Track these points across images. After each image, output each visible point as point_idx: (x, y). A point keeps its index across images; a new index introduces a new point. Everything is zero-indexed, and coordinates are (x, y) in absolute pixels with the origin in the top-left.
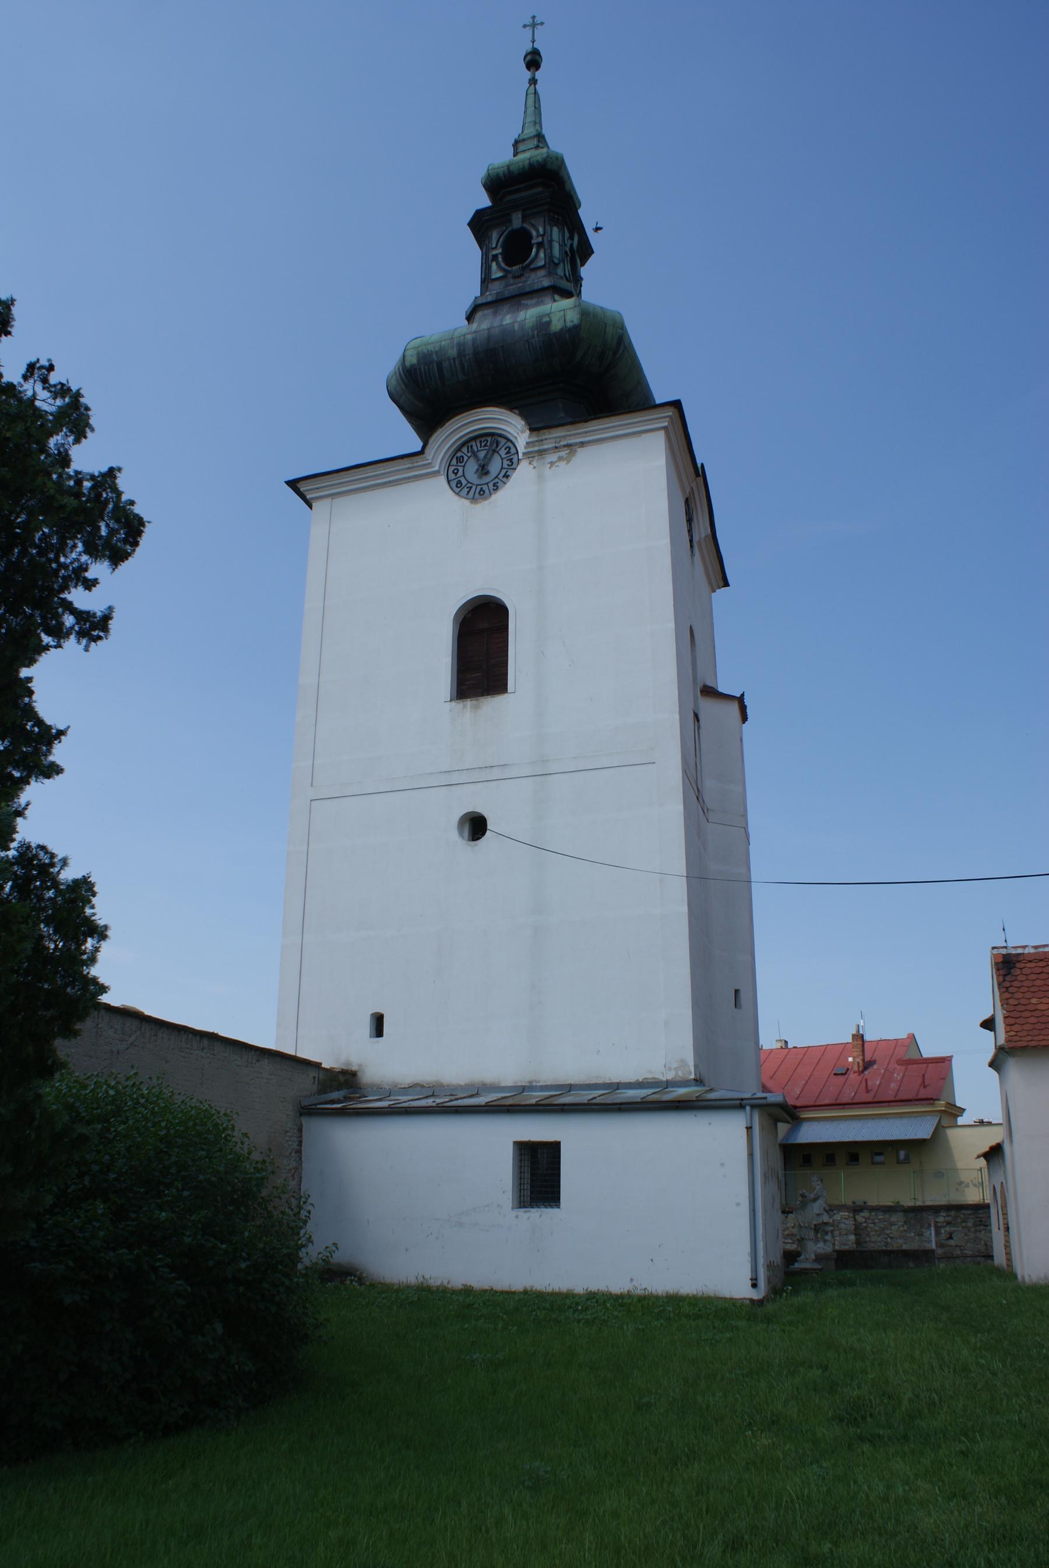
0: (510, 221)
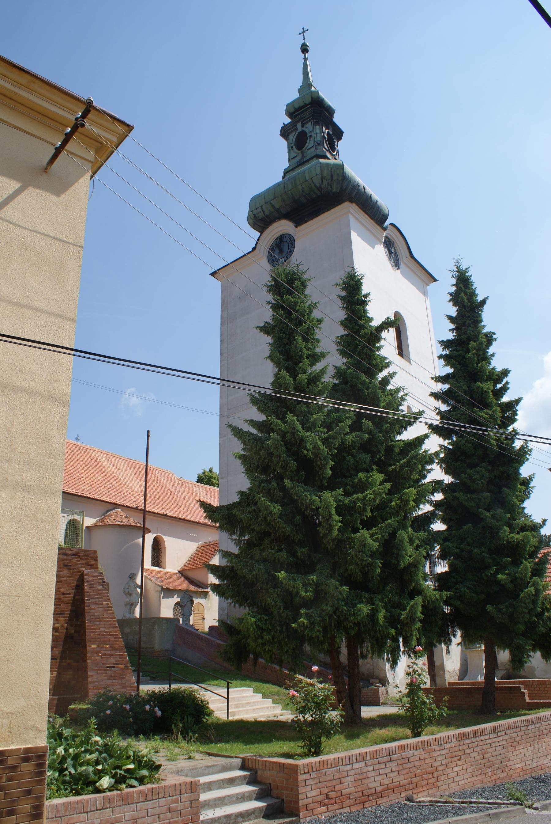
0: (297, 128)
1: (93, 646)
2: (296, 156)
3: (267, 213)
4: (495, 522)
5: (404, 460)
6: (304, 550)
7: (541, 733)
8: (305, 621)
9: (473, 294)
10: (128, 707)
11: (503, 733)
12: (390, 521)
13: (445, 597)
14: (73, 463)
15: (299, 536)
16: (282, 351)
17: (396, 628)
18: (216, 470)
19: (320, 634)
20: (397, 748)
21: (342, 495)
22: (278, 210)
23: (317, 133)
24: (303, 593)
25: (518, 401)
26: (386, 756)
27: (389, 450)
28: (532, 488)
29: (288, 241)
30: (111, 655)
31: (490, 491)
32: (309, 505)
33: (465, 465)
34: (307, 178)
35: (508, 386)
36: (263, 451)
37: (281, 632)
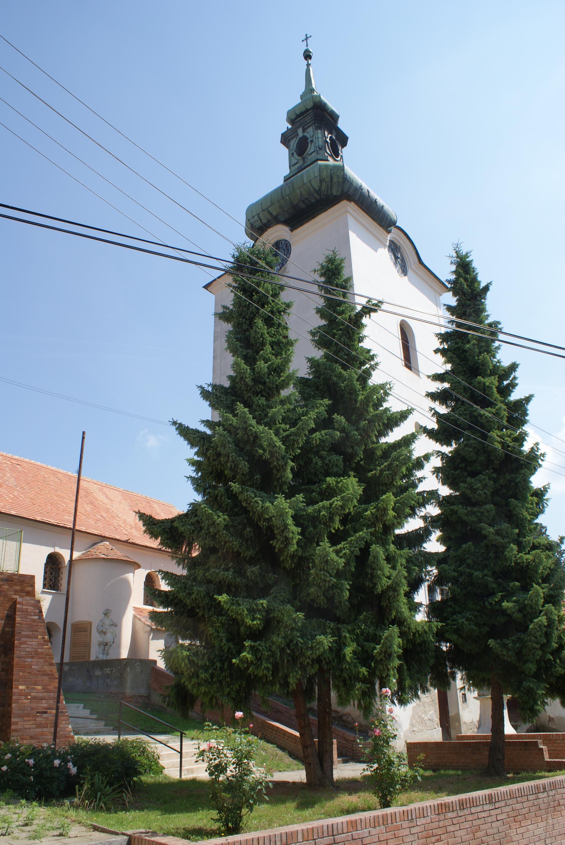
0: (298, 134)
1: (21, 687)
4: (499, 539)
5: (386, 464)
6: (254, 569)
7: (556, 803)
8: (248, 656)
9: (474, 280)
10: (31, 762)
11: (503, 804)
12: (361, 533)
13: (435, 630)
14: (59, 493)
15: (249, 553)
16: (241, 338)
17: (369, 667)
19: (268, 672)
20: (345, 825)
21: (303, 502)
23: (318, 138)
24: (249, 621)
25: (528, 399)
26: (329, 836)
27: (370, 454)
28: (547, 500)
29: (284, 247)
30: (42, 699)
31: (495, 504)
32: (262, 513)
33: (466, 474)
34: (305, 181)
35: (516, 382)
36: (211, 451)
37: (222, 669)
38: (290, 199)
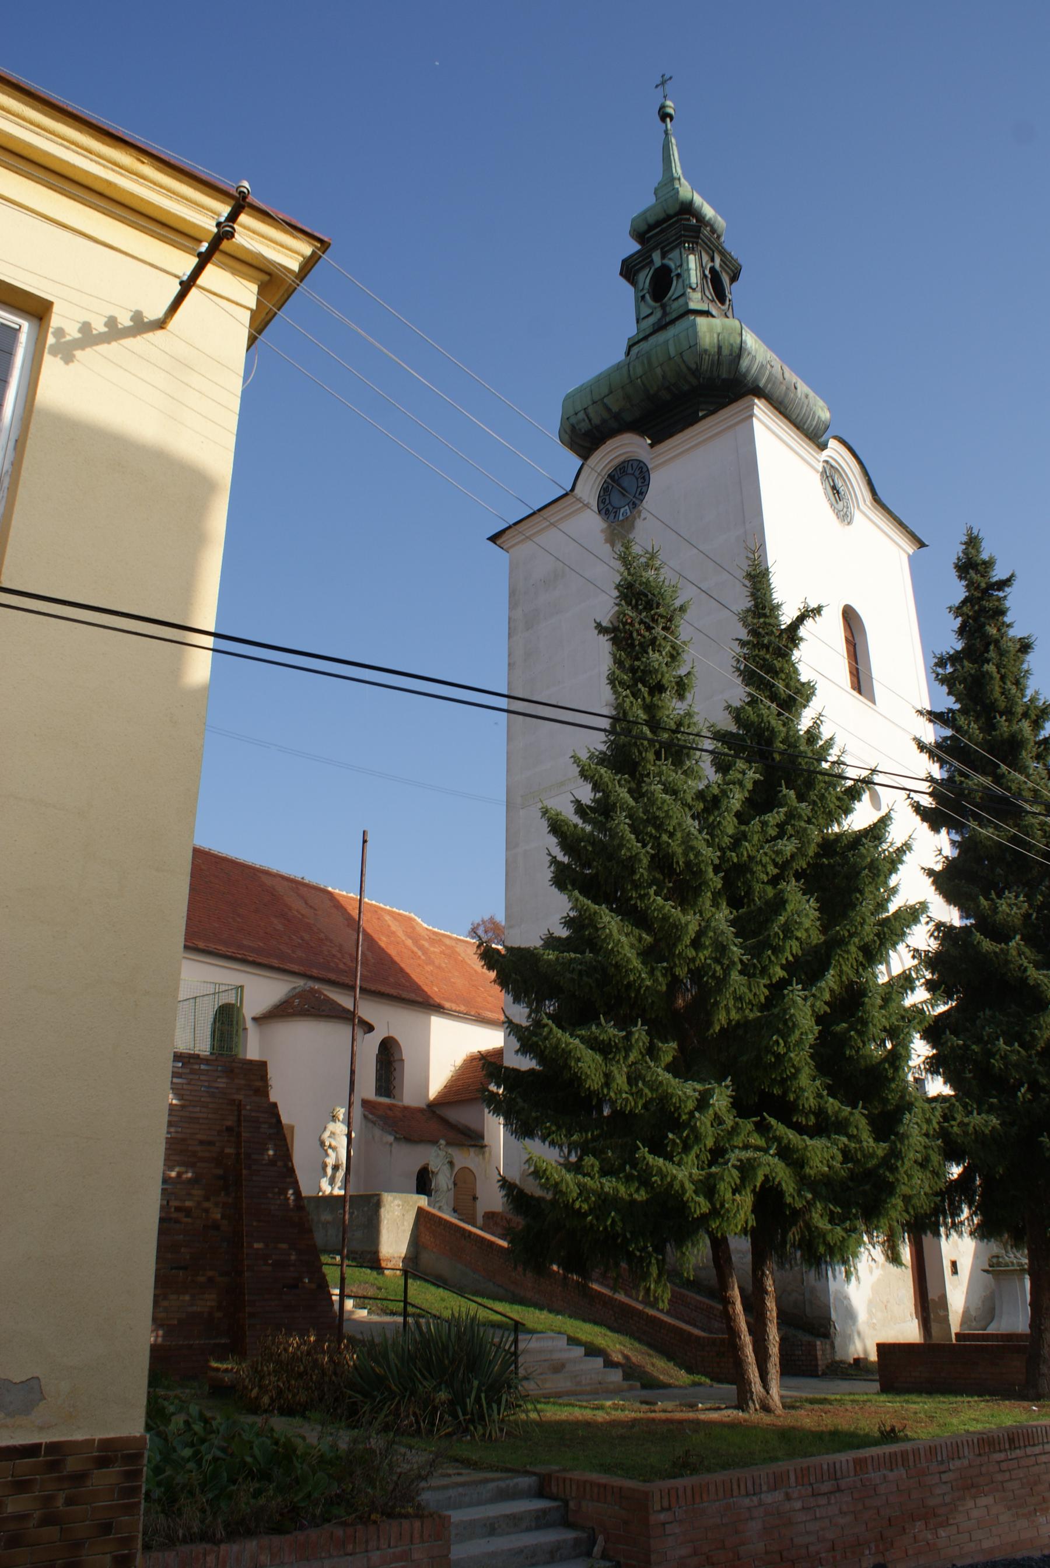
0: (652, 261)
2: (652, 313)
3: (596, 421)
18: (501, 918)
20: (851, 1464)
22: (616, 416)
29: (637, 473)
34: (672, 352)
38: (643, 383)
